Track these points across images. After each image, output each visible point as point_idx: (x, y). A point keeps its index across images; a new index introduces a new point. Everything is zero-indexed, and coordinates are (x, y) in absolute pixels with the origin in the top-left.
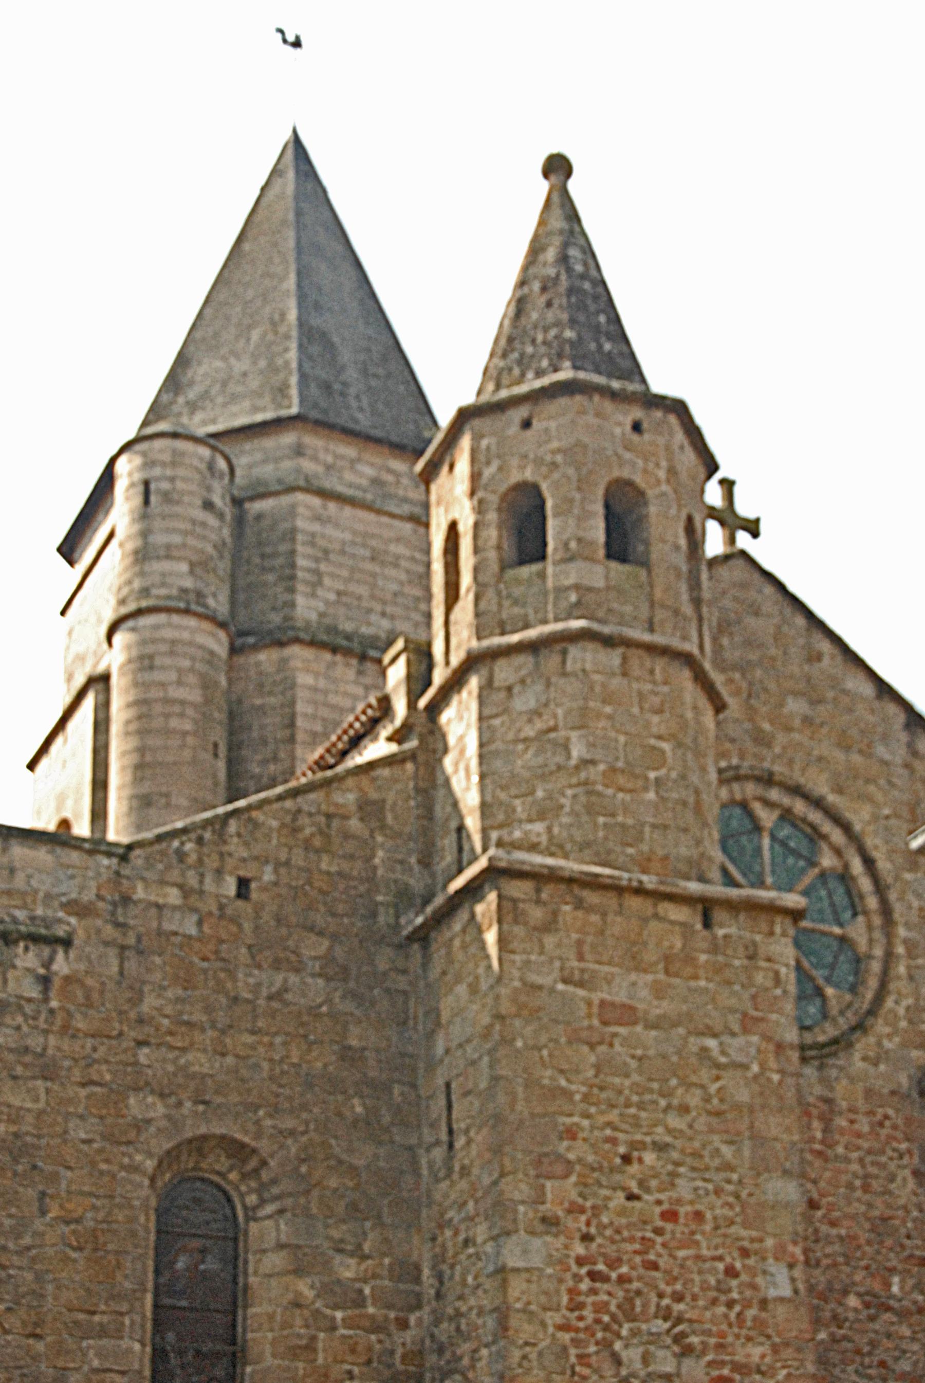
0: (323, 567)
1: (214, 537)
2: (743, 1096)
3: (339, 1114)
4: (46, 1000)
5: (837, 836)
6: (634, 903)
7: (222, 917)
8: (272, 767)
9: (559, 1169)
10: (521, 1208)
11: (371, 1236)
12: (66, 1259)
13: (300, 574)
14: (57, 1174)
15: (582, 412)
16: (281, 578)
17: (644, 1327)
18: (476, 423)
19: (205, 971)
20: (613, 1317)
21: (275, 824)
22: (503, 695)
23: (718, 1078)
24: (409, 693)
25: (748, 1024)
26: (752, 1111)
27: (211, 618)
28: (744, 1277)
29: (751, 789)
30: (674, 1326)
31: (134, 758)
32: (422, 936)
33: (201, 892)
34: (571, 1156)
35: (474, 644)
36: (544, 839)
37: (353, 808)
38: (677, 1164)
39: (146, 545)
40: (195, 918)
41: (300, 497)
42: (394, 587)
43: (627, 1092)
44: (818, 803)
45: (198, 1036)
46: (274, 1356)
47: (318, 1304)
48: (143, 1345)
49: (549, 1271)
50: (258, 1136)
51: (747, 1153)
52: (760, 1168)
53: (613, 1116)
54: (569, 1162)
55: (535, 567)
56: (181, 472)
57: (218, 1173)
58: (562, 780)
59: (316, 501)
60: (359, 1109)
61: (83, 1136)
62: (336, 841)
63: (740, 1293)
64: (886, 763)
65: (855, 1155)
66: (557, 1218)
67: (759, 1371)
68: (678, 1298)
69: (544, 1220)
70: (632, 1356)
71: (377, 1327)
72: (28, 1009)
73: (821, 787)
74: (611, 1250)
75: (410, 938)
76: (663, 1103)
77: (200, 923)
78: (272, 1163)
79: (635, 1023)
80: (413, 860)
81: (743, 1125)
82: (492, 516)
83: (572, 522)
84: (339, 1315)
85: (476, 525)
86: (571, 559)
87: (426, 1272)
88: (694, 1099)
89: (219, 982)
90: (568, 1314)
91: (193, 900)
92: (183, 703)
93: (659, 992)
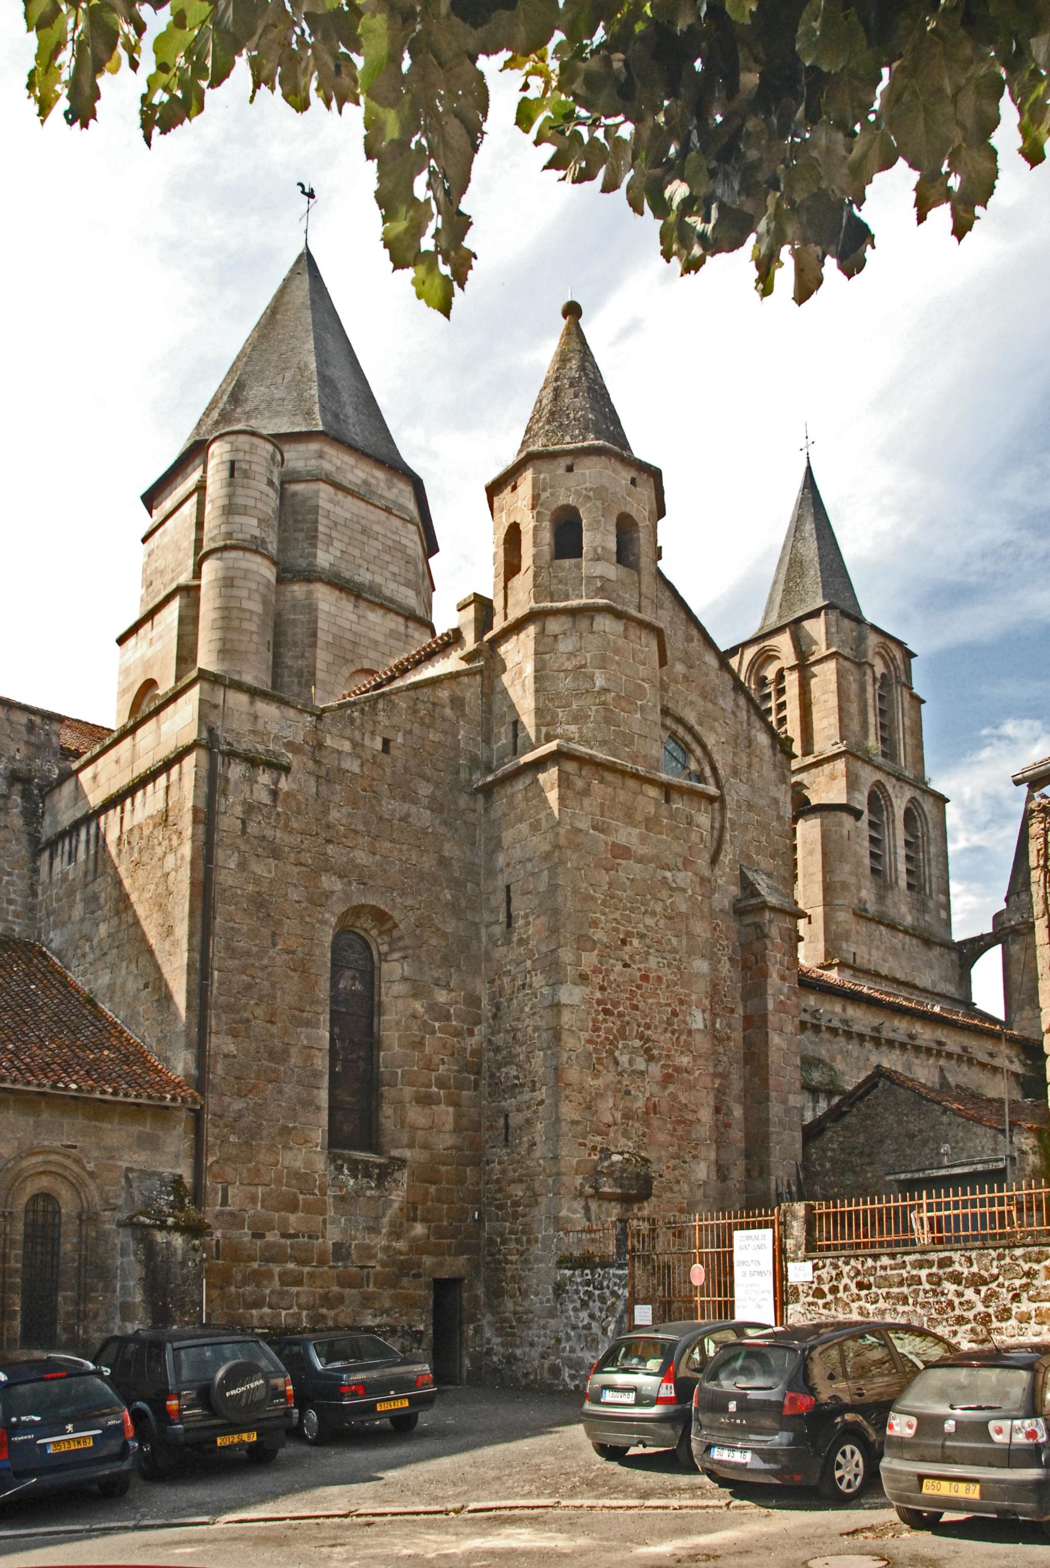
0: (334, 534)
2: (683, 908)
3: (438, 899)
4: (275, 806)
5: (698, 752)
6: (631, 783)
7: (374, 763)
8: (300, 662)
9: (589, 945)
11: (454, 977)
12: (288, 977)
13: (321, 536)
14: (281, 920)
15: (606, 468)
16: (307, 538)
18: (537, 463)
19: (365, 797)
20: (615, 1037)
21: (404, 706)
22: (551, 639)
23: (671, 896)
24: (476, 629)
25: (687, 864)
26: (687, 918)
28: (680, 1017)
31: (217, 645)
32: (487, 791)
33: (363, 745)
34: (595, 938)
35: (533, 604)
36: (577, 735)
37: (447, 701)
39: (230, 504)
40: (359, 762)
41: (322, 486)
42: (374, 552)
44: (690, 730)
45: (360, 840)
46: (400, 1046)
47: (426, 1017)
50: (394, 908)
51: (684, 943)
52: (690, 953)
53: (617, 915)
55: (573, 561)
56: (255, 458)
57: (365, 930)
58: (589, 700)
60: (449, 897)
62: (438, 721)
67: (686, 1071)
68: (648, 1027)
70: (624, 1059)
71: (458, 1034)
72: (265, 811)
73: (691, 718)
74: (614, 996)
75: (479, 790)
76: (643, 909)
77: (362, 766)
78: (401, 926)
80: (479, 739)
81: (683, 926)
82: (547, 524)
83: (599, 536)
84: (437, 1024)
85: (535, 528)
86: (598, 559)
87: (485, 1002)
88: (658, 908)
89: (372, 806)
91: (358, 750)
92: (251, 612)
93: (643, 840)
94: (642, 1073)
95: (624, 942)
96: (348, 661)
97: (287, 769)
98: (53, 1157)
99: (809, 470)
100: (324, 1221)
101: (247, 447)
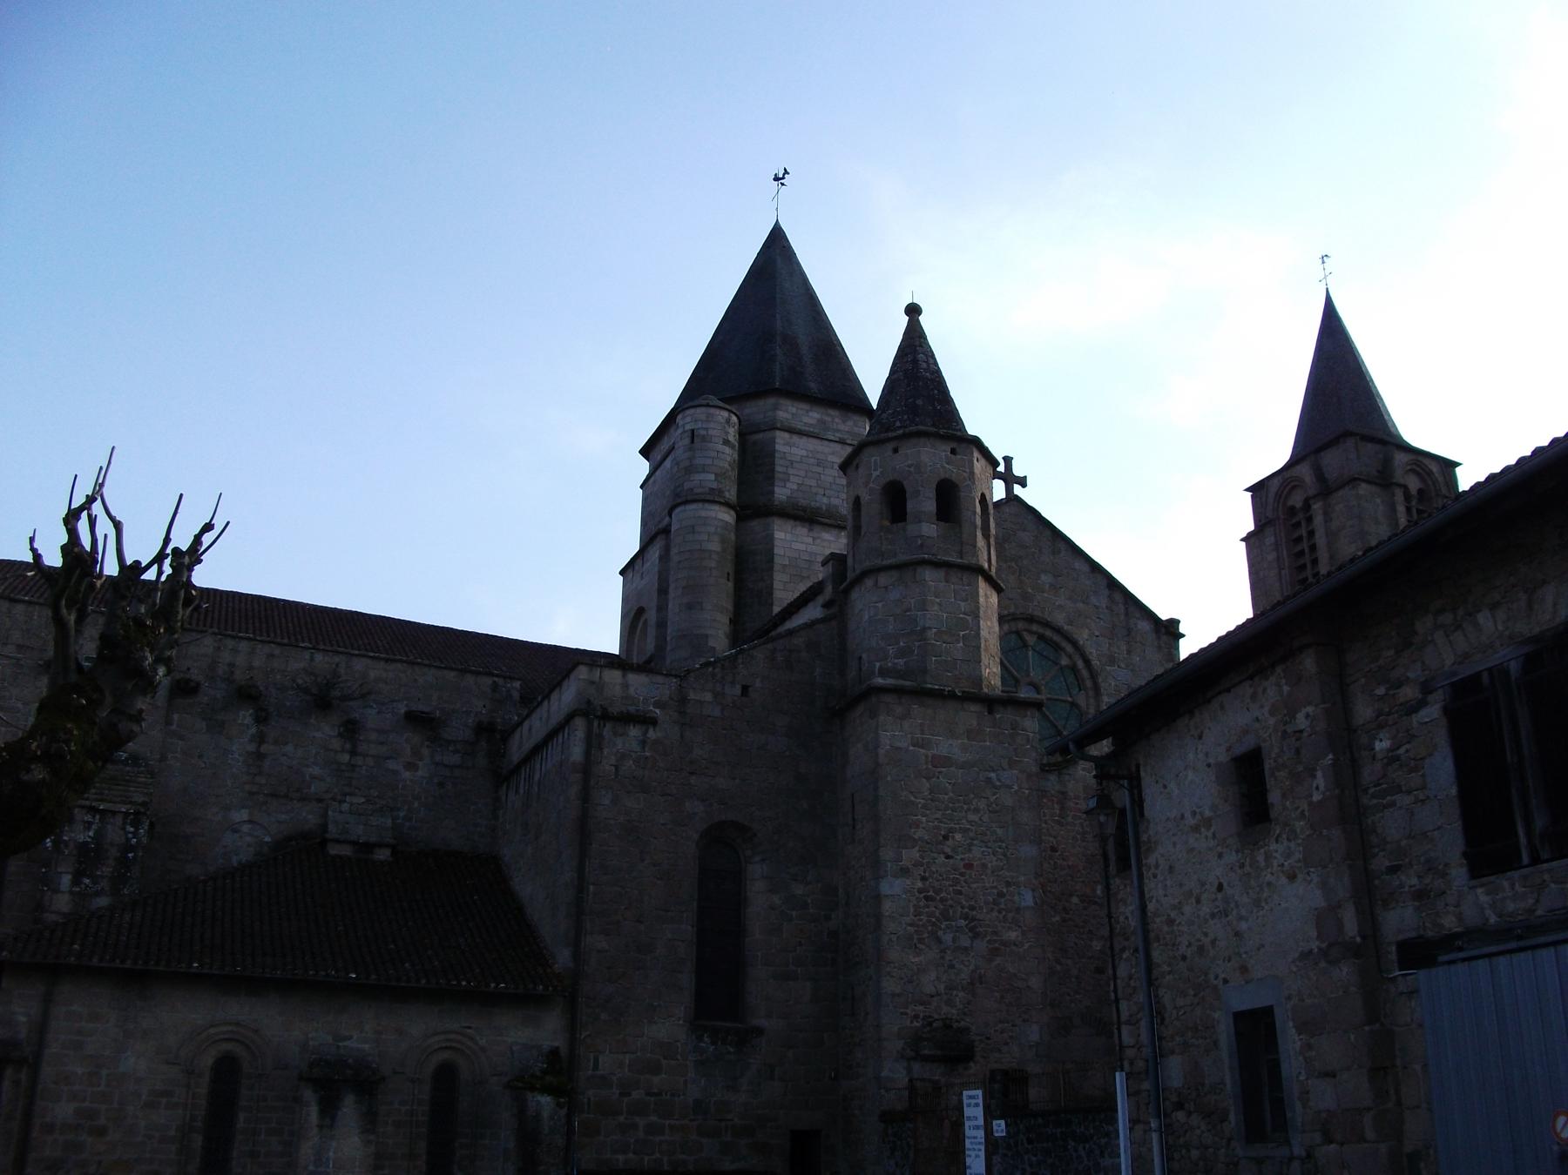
1: (729, 459)
5: (1069, 648)
10: (889, 864)
17: (954, 923)
20: (938, 920)
23: (994, 794)
27: (727, 504)
29: (1021, 625)
30: (970, 923)
34: (916, 837)
38: (973, 839)
42: (830, 479)
43: (946, 803)
44: (1058, 630)
48: (693, 927)
49: (904, 896)
53: (939, 815)
54: (914, 839)
56: (712, 425)
59: (786, 435)
61: (662, 822)
63: (1006, 905)
64: (1097, 607)
65: (1078, 822)
66: (908, 868)
67: (1015, 945)
68: (972, 908)
69: (902, 869)
79: (951, 766)
84: (794, 913)
90: (913, 918)
94: (966, 949)
95: (946, 838)
96: (803, 577)
97: (653, 722)
98: (452, 1036)
100: (686, 1082)
101: (703, 417)
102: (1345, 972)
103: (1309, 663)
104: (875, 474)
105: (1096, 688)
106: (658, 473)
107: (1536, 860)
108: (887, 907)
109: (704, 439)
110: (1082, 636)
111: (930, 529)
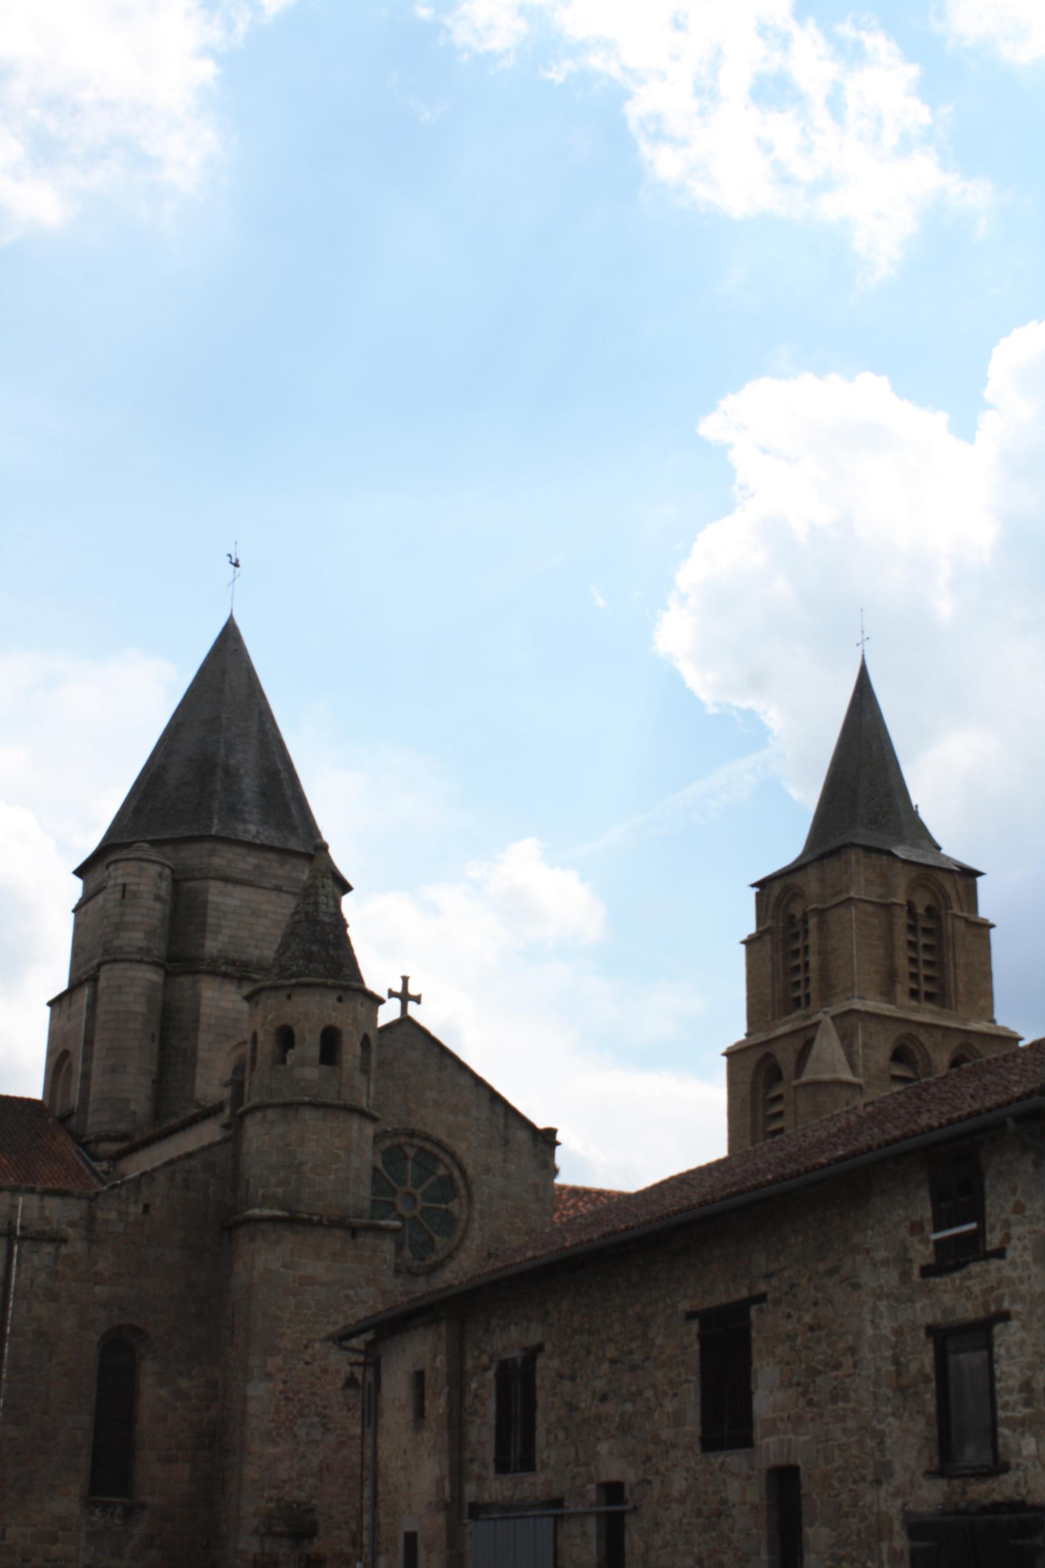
5: (447, 1160)
44: (438, 1144)
59: (220, 884)
68: (325, 1407)
70: (301, 1432)
76: (325, 1320)
84: (179, 1404)
95: (306, 1347)
97: (64, 1241)
99: (863, 656)
102: (441, 1518)
103: (443, 1329)
104: (270, 1017)
105: (470, 1197)
106: (90, 904)
107: (515, 1471)
108: (252, 1407)
109: (135, 895)
110: (461, 1148)
111: (312, 1073)
